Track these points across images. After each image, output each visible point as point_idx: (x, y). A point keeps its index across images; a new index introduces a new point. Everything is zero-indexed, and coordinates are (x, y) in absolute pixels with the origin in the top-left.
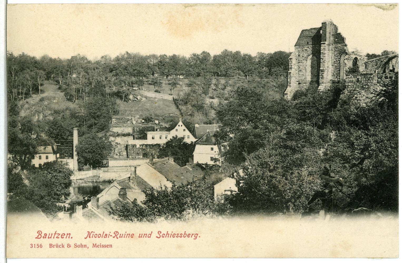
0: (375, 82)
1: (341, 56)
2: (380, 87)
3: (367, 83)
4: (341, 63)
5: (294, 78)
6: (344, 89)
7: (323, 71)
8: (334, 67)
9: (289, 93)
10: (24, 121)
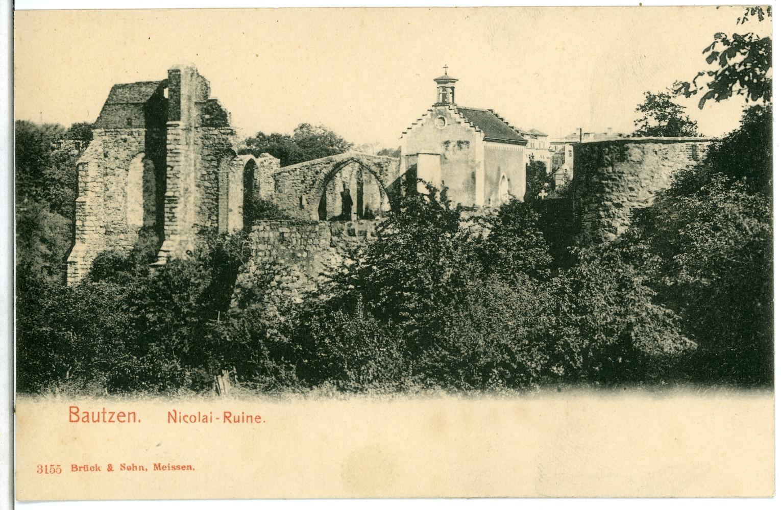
0: (324, 242)
1: (219, 161)
2: (336, 255)
3: (305, 246)
4: (220, 179)
5: (94, 218)
6: (246, 260)
7: (173, 200)
8: (202, 189)
9: (79, 260)
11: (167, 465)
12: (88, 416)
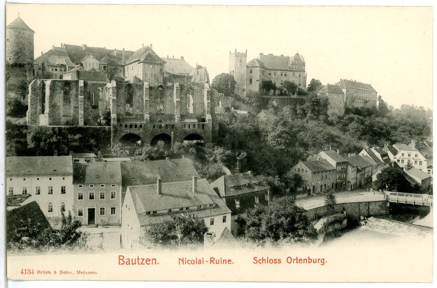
10: (30, 117)
11: (83, 272)
12: (129, 261)
